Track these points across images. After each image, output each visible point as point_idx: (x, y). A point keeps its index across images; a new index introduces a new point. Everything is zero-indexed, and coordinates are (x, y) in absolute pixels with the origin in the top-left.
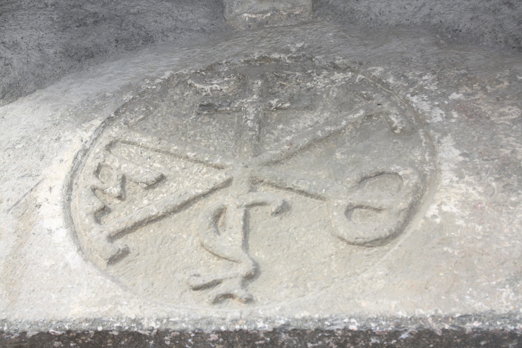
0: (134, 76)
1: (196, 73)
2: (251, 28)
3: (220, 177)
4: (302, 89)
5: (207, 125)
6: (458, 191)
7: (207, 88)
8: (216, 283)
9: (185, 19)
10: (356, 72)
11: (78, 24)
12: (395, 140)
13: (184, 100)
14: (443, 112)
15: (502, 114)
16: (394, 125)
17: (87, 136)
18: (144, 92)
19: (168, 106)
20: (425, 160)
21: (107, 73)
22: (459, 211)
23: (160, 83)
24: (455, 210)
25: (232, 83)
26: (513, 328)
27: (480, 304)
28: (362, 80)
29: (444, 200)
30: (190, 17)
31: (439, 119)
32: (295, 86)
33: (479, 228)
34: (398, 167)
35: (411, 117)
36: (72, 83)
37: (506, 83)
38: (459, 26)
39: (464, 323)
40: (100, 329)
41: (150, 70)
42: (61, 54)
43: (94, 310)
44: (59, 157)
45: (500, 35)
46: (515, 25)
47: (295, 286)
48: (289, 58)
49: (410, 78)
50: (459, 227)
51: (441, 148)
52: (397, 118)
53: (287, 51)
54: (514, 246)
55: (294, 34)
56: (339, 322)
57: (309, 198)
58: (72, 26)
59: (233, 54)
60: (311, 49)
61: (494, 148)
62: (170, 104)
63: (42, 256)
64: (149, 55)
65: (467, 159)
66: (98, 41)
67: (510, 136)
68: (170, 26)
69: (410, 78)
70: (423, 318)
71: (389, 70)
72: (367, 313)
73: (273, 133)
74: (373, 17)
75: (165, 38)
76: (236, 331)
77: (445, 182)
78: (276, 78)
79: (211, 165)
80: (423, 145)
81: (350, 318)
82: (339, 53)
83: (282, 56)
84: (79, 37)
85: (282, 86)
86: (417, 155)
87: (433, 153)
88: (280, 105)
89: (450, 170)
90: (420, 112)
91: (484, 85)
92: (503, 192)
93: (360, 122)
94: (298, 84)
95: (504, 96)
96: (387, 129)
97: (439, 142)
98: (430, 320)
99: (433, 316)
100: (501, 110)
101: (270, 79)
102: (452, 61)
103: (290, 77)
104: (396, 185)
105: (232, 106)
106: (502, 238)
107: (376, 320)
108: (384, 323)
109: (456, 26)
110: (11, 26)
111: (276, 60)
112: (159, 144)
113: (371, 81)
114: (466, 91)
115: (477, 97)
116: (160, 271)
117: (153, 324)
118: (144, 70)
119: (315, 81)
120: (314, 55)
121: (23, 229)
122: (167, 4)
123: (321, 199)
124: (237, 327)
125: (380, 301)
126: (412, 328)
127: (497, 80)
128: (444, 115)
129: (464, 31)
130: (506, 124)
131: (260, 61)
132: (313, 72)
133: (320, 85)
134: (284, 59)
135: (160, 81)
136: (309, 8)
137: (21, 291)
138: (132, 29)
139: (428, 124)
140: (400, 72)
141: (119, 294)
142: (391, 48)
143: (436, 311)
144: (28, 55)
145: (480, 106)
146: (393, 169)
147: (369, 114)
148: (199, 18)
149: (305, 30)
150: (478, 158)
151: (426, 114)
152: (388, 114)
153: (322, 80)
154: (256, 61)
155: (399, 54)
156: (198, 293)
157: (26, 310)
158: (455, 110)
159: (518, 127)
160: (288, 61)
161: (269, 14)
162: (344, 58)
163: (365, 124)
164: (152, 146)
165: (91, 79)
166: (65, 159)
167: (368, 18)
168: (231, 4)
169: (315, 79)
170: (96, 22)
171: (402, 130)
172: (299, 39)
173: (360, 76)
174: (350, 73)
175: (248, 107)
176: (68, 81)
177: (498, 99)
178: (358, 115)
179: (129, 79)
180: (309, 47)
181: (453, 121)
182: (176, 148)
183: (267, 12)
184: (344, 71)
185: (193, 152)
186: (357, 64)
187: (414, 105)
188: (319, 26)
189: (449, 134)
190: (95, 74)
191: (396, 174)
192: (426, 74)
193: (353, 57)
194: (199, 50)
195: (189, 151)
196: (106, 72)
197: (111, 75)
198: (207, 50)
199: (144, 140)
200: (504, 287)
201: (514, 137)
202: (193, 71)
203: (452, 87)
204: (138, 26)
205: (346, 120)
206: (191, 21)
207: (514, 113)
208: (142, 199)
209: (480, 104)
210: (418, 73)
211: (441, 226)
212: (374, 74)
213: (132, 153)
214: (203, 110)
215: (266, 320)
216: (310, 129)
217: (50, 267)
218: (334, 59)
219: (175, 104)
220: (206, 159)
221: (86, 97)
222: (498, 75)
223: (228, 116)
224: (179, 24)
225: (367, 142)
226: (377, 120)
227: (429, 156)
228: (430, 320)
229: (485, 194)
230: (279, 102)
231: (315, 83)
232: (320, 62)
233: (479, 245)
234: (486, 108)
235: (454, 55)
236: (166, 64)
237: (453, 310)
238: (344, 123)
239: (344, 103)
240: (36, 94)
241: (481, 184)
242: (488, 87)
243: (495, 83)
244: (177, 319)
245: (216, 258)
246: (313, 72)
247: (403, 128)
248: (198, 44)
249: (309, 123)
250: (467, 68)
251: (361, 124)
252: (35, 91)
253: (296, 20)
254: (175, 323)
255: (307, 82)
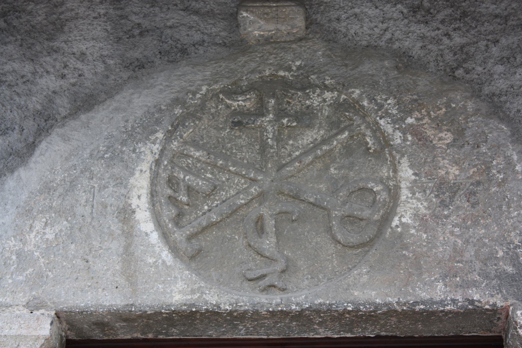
0: (179, 89)
1: (225, 87)
2: (261, 43)
3: (255, 190)
4: (303, 107)
5: (239, 139)
6: (411, 206)
7: (235, 104)
8: (263, 277)
9: (209, 31)
10: (340, 93)
11: (128, 36)
12: (370, 158)
13: (219, 113)
14: (401, 135)
15: (440, 139)
16: (369, 146)
17: (156, 148)
18: (189, 106)
19: (208, 119)
20: (390, 176)
21: (158, 85)
22: (412, 222)
23: (200, 98)
24: (410, 221)
25: (253, 100)
26: (443, 309)
27: (424, 293)
28: (345, 100)
29: (403, 213)
30: (213, 31)
31: (399, 141)
32: (298, 103)
33: (425, 236)
34: (373, 184)
35: (380, 137)
36: (133, 94)
37: (444, 110)
38: (412, 53)
39: (415, 306)
40: (194, 310)
41: (190, 83)
42: (120, 66)
43: (189, 297)
44: (139, 168)
45: (441, 64)
46: (452, 55)
47: (312, 278)
48: (291, 76)
49: (379, 101)
50: (412, 235)
51: (400, 168)
52: (371, 140)
53: (289, 69)
54: (445, 251)
55: (293, 51)
56: (340, 305)
57: (315, 207)
58: (123, 37)
59: (250, 70)
60: (307, 68)
61: (435, 169)
62: (209, 116)
63: (145, 254)
64: (187, 68)
65: (417, 178)
66: (146, 53)
67: (446, 159)
68: (199, 39)
69: (379, 101)
70: (390, 303)
71: (364, 92)
72: (358, 299)
73: (286, 149)
74: (350, 37)
75: (197, 51)
76: (278, 311)
77: (403, 198)
78: (283, 96)
79: (247, 178)
80: (389, 163)
81: (348, 304)
82: (327, 72)
83: (287, 73)
84: (131, 49)
85: (289, 103)
86: (385, 172)
87: (395, 171)
88: (289, 124)
89: (407, 188)
90: (386, 135)
91: (429, 110)
92: (439, 207)
93: (346, 141)
94: (300, 102)
95: (442, 121)
96: (364, 148)
97: (399, 162)
98: (395, 305)
99: (397, 302)
100: (440, 135)
101: (279, 96)
102: (408, 86)
103: (294, 97)
104: (371, 198)
105: (255, 123)
106: (439, 244)
107: (364, 305)
108: (368, 306)
109: (411, 53)
110: (76, 37)
111: (281, 77)
112: (209, 158)
113: (351, 101)
114: (417, 116)
115: (424, 122)
116: (225, 265)
117: (227, 307)
118: (185, 83)
119: (311, 99)
120: (309, 74)
121: (127, 231)
122: (194, 17)
123: (323, 209)
124: (280, 309)
125: (365, 291)
126: (385, 309)
127: (437, 107)
128: (402, 138)
129: (416, 57)
130: (443, 148)
131: (270, 76)
132: (310, 92)
133: (316, 103)
134: (288, 76)
135: (200, 96)
136: (303, 28)
137: (35, 61)
138: (170, 42)
139: (392, 145)
140: (372, 95)
141: (202, 285)
142: (364, 70)
143: (399, 299)
144: (95, 66)
145: (426, 131)
146: (369, 186)
147: (352, 135)
148: (220, 31)
149: (301, 47)
150: (425, 178)
151: (390, 137)
152: (364, 136)
153: (316, 98)
154: (267, 77)
155: (370, 77)
156: (252, 283)
157: (145, 297)
158: (410, 134)
159: (450, 151)
160: (291, 78)
161: (274, 32)
162: (331, 79)
163: (349, 143)
164: (203, 159)
165: (147, 90)
166: (144, 170)
167: (347, 38)
168: (245, 22)
169: (311, 97)
170: (141, 34)
171: (374, 150)
172: (297, 57)
173: (343, 96)
174: (336, 93)
175: (267, 125)
176: (129, 91)
177: (438, 125)
178: (344, 136)
179: (176, 92)
180: (305, 66)
181: (408, 143)
182: (221, 162)
183: (273, 31)
184: (332, 90)
185: (234, 167)
186: (341, 86)
187: (382, 127)
188: (311, 44)
189: (406, 156)
190: (148, 85)
191: (372, 190)
192: (389, 99)
193: (338, 78)
194: (224, 64)
195: (230, 166)
196: (157, 83)
197: (161, 87)
198: (230, 65)
199: (198, 154)
200: (439, 282)
201: (448, 160)
202: (222, 86)
203: (407, 111)
204: (175, 39)
205: (336, 140)
206: (214, 34)
207: (449, 138)
208: (203, 205)
209: (426, 129)
210: (384, 97)
211: (401, 234)
212: (353, 96)
213: (190, 164)
214: (235, 126)
215: (297, 304)
216: (311, 145)
217: (153, 264)
218: (325, 79)
219: (213, 118)
220: (244, 173)
221: (146, 109)
222: (439, 102)
223: (253, 131)
224: (206, 38)
225: (351, 159)
226: (357, 139)
227: (392, 172)
228: (395, 305)
229: (428, 208)
230: (288, 121)
231: (312, 101)
232: (314, 81)
233: (425, 249)
234: (430, 133)
235: (409, 80)
236: (201, 78)
237: (409, 298)
238: (335, 143)
239: (333, 122)
240: (108, 102)
241: (426, 200)
242: (432, 113)
243: (436, 109)
244: (242, 304)
245: (259, 256)
246: (310, 92)
247: (376, 149)
248: (222, 58)
249: (310, 140)
250: (418, 93)
251: (346, 143)
252: (106, 100)
253: (294, 36)
254: (241, 306)
255: (306, 100)
